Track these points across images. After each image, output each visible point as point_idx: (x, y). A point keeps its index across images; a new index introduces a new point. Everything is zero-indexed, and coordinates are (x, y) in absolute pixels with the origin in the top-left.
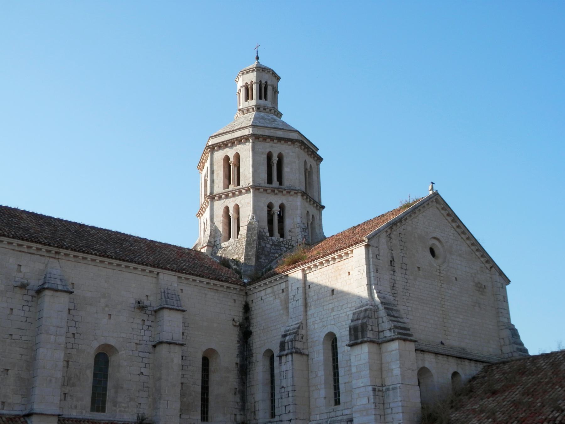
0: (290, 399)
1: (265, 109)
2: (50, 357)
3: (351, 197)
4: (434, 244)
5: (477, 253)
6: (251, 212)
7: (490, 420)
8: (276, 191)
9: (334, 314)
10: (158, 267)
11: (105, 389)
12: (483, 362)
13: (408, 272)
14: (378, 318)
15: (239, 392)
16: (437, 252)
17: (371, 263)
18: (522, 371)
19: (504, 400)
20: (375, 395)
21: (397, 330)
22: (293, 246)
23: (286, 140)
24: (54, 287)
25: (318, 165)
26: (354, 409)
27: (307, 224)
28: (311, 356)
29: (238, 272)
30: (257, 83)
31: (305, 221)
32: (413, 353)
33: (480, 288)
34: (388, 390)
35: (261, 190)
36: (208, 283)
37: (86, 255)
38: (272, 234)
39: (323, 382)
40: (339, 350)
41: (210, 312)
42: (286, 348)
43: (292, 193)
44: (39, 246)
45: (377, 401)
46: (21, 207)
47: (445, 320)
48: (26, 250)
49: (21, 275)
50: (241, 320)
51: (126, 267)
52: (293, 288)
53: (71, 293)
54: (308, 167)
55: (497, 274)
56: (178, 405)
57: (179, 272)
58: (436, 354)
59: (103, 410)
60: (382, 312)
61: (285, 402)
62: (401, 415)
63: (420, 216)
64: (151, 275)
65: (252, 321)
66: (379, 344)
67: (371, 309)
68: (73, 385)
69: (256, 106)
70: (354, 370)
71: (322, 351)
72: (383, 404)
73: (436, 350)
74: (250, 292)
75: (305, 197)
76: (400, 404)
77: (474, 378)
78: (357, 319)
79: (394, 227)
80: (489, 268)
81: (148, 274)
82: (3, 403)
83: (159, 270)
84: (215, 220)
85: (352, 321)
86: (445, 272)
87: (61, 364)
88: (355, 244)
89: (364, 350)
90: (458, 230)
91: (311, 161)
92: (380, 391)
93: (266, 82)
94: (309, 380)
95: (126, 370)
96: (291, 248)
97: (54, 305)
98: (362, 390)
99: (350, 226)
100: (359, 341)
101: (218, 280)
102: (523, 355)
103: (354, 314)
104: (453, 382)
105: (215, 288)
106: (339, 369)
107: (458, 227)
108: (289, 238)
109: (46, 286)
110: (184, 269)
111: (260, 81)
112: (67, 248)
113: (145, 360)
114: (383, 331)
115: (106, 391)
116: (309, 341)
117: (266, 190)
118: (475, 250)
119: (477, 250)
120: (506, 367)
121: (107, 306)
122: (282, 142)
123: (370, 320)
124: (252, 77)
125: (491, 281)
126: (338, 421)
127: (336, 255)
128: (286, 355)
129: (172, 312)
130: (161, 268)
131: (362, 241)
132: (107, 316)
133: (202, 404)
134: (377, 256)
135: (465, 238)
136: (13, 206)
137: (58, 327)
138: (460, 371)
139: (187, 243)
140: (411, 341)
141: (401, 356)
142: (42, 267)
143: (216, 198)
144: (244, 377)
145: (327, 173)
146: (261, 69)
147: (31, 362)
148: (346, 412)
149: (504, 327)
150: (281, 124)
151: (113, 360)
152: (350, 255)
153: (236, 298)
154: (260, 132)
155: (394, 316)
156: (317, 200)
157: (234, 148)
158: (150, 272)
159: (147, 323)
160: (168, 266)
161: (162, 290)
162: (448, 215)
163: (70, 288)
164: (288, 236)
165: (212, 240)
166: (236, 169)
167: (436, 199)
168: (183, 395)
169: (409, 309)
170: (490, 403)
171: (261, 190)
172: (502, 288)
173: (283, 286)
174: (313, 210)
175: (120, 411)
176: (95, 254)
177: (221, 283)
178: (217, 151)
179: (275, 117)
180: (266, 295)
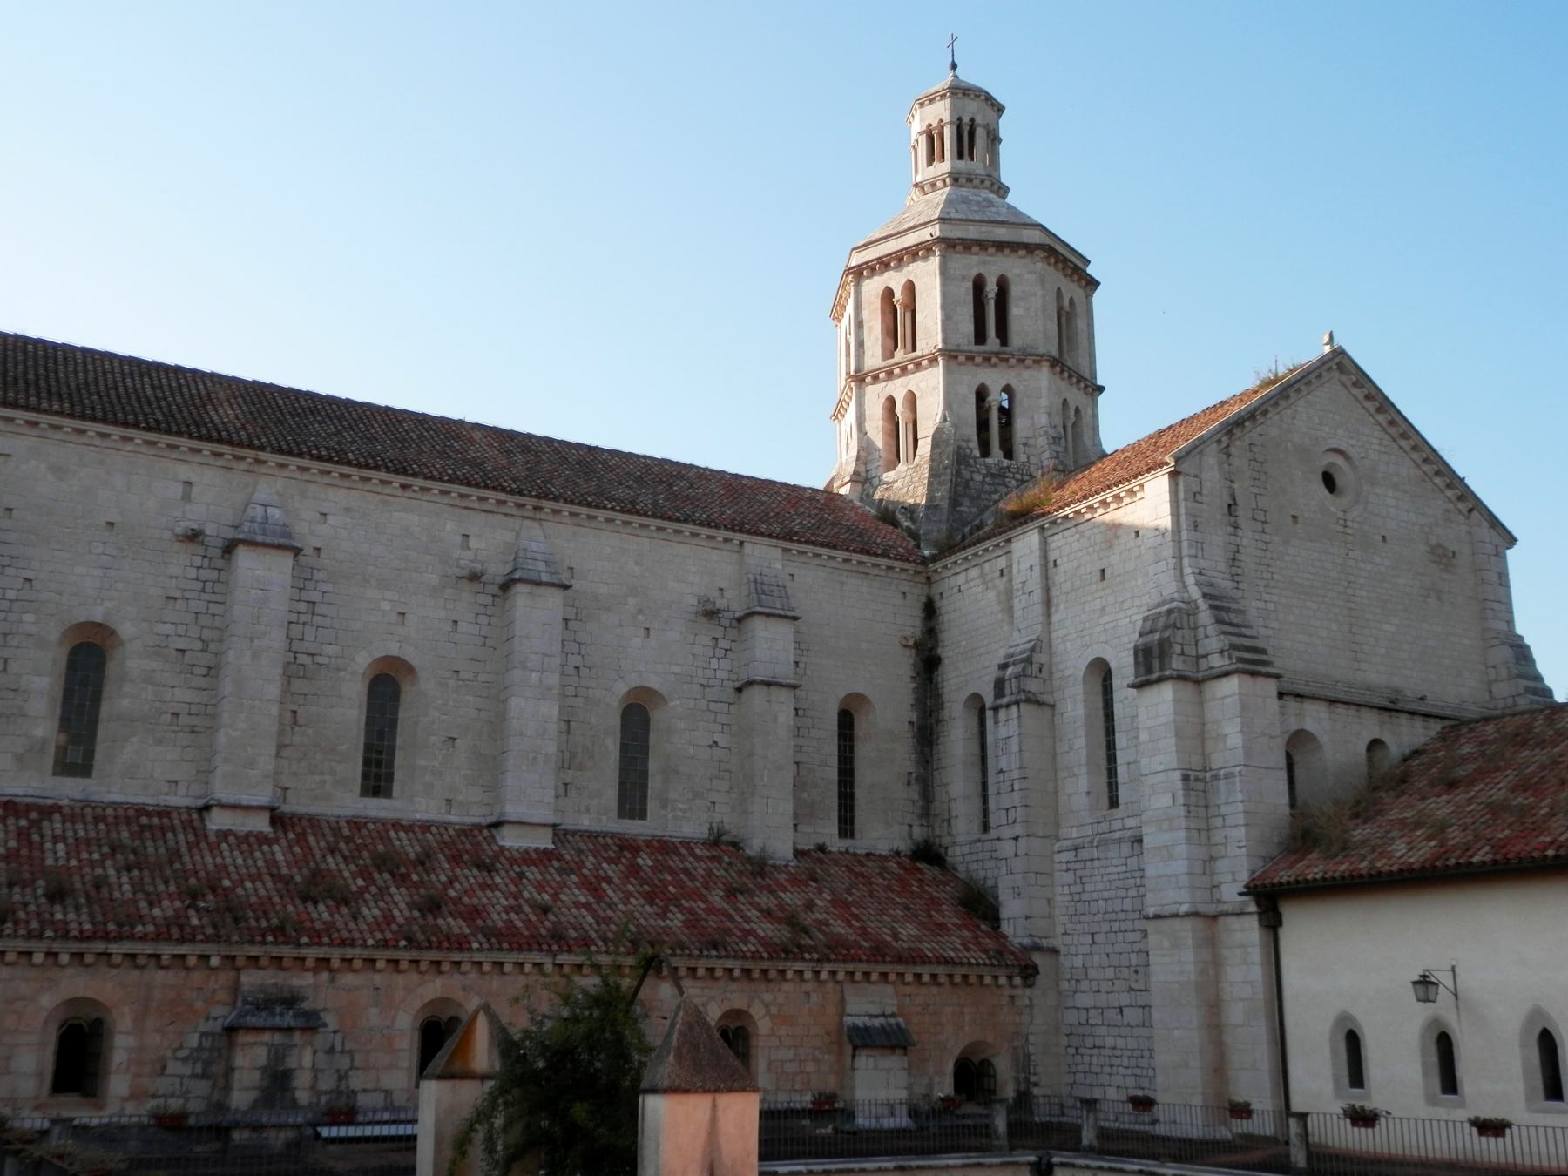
0: (1016, 796)
1: (970, 180)
2: (533, 713)
3: (1158, 369)
4: (1332, 464)
5: (1438, 480)
6: (941, 407)
7: (1433, 843)
8: (994, 360)
9: (1105, 619)
10: (741, 531)
11: (644, 774)
12: (1442, 718)
13: (1268, 528)
14: (1196, 628)
15: (916, 779)
16: (1340, 481)
17: (1182, 511)
18: (1521, 739)
19: (1470, 801)
20: (1187, 789)
21: (1236, 654)
22: (1031, 477)
23: (1014, 247)
24: (534, 576)
25: (1089, 297)
26: (1144, 818)
27: (1065, 428)
28: (1059, 708)
29: (914, 535)
30: (951, 123)
31: (1058, 421)
32: (1274, 704)
33: (1443, 557)
34: (1216, 778)
35: (962, 358)
36: (846, 561)
37: (593, 512)
38: (985, 451)
39: (1084, 760)
40: (1117, 696)
41: (856, 617)
42: (1008, 691)
43: (1029, 362)
44: (502, 496)
45: (1193, 800)
46: (472, 418)
47: (1355, 630)
48: (476, 505)
49: (469, 555)
50: (918, 634)
51: (677, 532)
52: (1023, 567)
53: (567, 587)
54: (1066, 303)
55: (1485, 524)
56: (788, 807)
57: (784, 538)
58: (1332, 702)
59: (642, 814)
60: (1205, 616)
61: (1006, 801)
62: (1243, 830)
63: (1301, 402)
64: (728, 546)
65: (942, 636)
66: (1198, 682)
67: (1180, 610)
68: (581, 768)
69: (950, 174)
70: (1144, 737)
71: (1081, 697)
72: (1207, 807)
73: (1331, 695)
74: (935, 577)
75: (1058, 369)
76: (1241, 807)
77: (1417, 753)
78: (1151, 632)
79: (1237, 432)
80: (1465, 511)
81: (722, 546)
82: (449, 801)
83: (744, 537)
84: (868, 426)
85: (1141, 635)
86: (1355, 525)
87: (553, 728)
88: (1148, 471)
89: (1165, 695)
90: (1392, 430)
91: (1071, 289)
92: (1198, 782)
93: (972, 120)
94: (1054, 756)
95: (681, 737)
96: (1026, 478)
97: (535, 614)
98: (1161, 777)
99: (1152, 429)
100: (1154, 676)
101: (868, 553)
102: (1538, 702)
103: (1145, 619)
104: (1369, 759)
105: (861, 569)
106: (1117, 735)
107: (1392, 423)
108: (1023, 458)
109: (517, 575)
110: (796, 533)
111: (960, 119)
112: (556, 499)
113: (722, 718)
114: (1206, 656)
115: (646, 779)
116: (1056, 676)
117: (972, 358)
118: (1431, 473)
119: (1438, 473)
120: (1490, 728)
121: (640, 611)
122: (1007, 251)
123: (1179, 633)
124: (941, 111)
125: (1467, 539)
126: (1114, 841)
127: (1108, 496)
128: (1008, 706)
129: (772, 621)
130: (748, 532)
131: (1163, 464)
132: (642, 632)
133: (840, 805)
134: (1195, 496)
135: (1407, 448)
136: (455, 416)
137: (544, 655)
138: (1387, 738)
139: (811, 476)
140: (1268, 675)
141: (1244, 708)
142: (509, 537)
143: (869, 379)
144: (927, 750)
145: (1110, 318)
146: (960, 92)
147: (496, 725)
148: (1131, 822)
149: (1496, 642)
150: (1004, 210)
151: (657, 717)
152: (1139, 495)
153: (906, 589)
154: (957, 232)
155: (1231, 624)
156: (1087, 375)
157: (906, 270)
158: (726, 540)
159: (723, 644)
160: (763, 527)
161: (751, 577)
162: (1368, 397)
163: (564, 578)
164: (1021, 455)
165: (862, 469)
166: (908, 315)
167: (1338, 364)
168: (798, 786)
169: (1271, 606)
170: (1440, 807)
171: (962, 358)
172: (1497, 554)
173: (1002, 563)
174: (1076, 397)
175: (675, 818)
176: (613, 509)
177: (874, 560)
178: (869, 277)
179: (992, 196)
180: (967, 582)
